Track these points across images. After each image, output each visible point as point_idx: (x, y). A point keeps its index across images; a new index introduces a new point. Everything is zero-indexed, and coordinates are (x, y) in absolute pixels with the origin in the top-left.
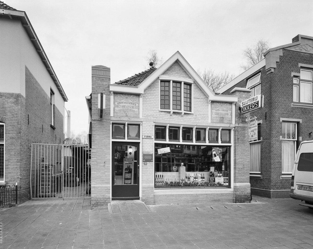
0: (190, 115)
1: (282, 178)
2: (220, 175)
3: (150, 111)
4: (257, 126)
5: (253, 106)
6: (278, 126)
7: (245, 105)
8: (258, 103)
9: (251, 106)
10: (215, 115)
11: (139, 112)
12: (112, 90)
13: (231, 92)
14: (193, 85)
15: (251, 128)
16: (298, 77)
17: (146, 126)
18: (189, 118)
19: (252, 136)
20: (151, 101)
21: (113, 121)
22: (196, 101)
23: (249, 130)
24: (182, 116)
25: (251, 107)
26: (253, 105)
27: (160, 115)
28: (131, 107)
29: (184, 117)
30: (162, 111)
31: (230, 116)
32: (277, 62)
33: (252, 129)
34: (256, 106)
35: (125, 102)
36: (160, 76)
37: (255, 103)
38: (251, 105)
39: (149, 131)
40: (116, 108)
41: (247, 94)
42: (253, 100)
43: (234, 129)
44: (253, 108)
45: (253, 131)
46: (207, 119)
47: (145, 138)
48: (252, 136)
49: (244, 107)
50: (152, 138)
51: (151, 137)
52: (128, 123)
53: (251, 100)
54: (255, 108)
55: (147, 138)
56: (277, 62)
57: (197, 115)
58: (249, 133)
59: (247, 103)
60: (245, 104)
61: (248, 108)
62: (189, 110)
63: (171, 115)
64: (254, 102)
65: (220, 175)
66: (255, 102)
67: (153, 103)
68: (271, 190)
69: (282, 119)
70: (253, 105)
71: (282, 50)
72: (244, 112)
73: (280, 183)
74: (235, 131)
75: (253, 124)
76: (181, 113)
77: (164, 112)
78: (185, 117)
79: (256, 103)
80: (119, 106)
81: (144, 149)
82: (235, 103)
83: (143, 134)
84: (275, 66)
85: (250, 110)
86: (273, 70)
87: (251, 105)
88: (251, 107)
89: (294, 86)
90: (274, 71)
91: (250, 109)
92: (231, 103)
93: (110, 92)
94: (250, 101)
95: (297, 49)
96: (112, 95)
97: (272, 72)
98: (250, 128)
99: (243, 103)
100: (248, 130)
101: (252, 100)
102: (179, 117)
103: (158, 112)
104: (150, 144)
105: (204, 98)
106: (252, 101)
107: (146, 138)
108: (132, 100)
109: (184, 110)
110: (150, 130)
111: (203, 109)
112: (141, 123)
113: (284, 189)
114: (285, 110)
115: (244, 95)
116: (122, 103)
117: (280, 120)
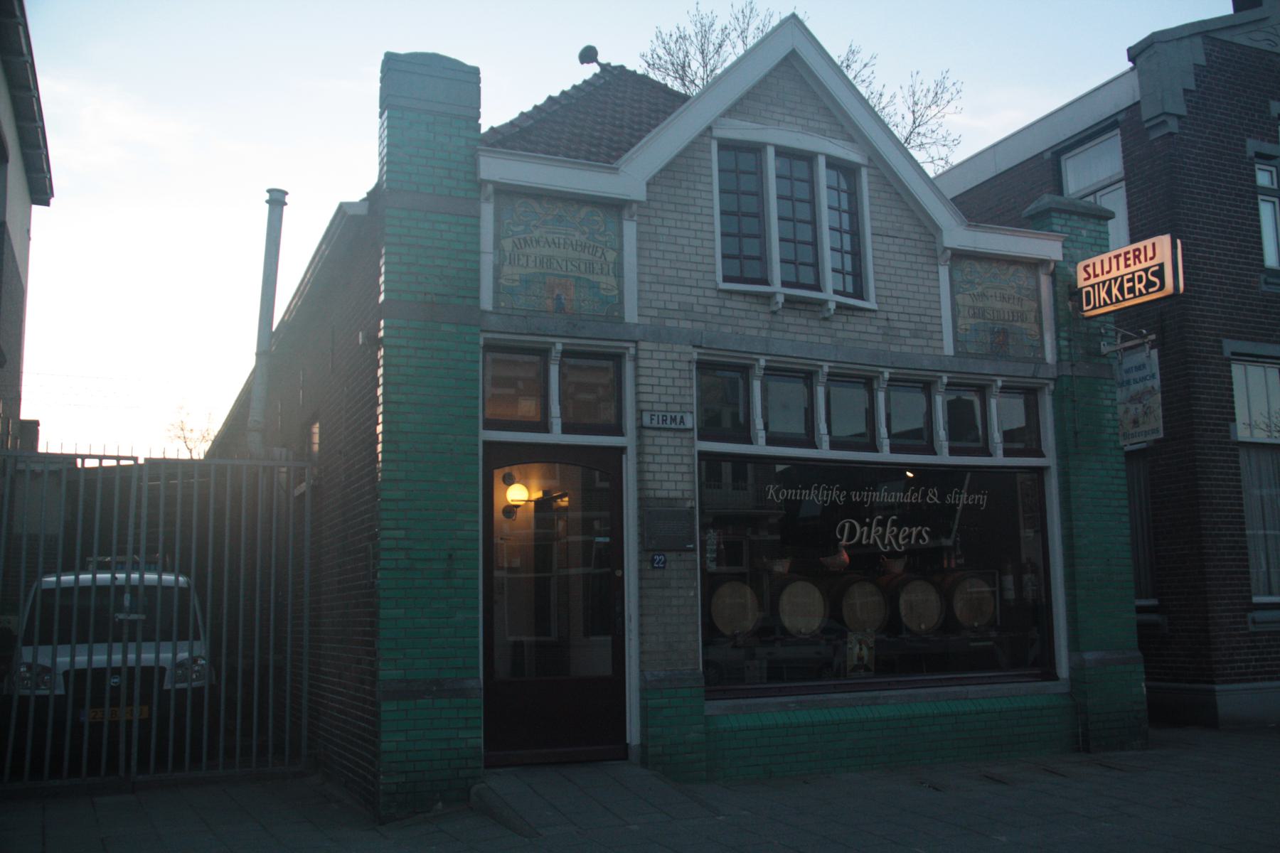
0: (860, 314)
1: (1254, 622)
2: (35, 657)
3: (674, 289)
4: (1158, 376)
5: (1137, 286)
6: (1214, 376)
7: (1101, 279)
8: (1160, 273)
9: (1126, 285)
10: (972, 321)
11: (621, 293)
12: (492, 178)
13: (1026, 212)
14: (864, 172)
15: (1128, 383)
16: (1272, 162)
17: (656, 364)
18: (859, 328)
19: (1135, 423)
20: (680, 241)
21: (489, 335)
22: (884, 247)
23: (1121, 395)
24: (826, 319)
25: (1131, 290)
26: (1140, 282)
27: (724, 312)
28: (583, 267)
29: (835, 326)
30: (730, 292)
31: (1035, 327)
32: (1186, 91)
33: (1135, 388)
34: (1154, 284)
35: (550, 240)
36: (715, 121)
37: (1146, 270)
38: (1128, 281)
39: (670, 391)
40: (507, 270)
41: (1098, 228)
42: (1137, 257)
43: (1052, 387)
44: (1141, 294)
45: (1136, 399)
46: (936, 336)
47: (655, 424)
48: (1135, 423)
49: (1093, 286)
50: (689, 424)
51: (682, 421)
52: (564, 344)
53: (1127, 259)
54: (1148, 293)
55: (673, 426)
56: (1186, 91)
57: (891, 316)
58: (1121, 409)
59: (1106, 268)
60: (1098, 271)
61: (1115, 291)
62: (850, 289)
63: (774, 313)
64: (1139, 266)
65: (35, 657)
66: (1144, 265)
67: (687, 250)
68: (1217, 687)
69: (1229, 346)
70: (1140, 282)
71: (1198, 40)
72: (1094, 308)
73: (1248, 647)
74: (1058, 398)
75: (1141, 367)
76: (823, 303)
77: (741, 298)
78: (840, 326)
79: (1153, 274)
80: (523, 261)
81: (650, 485)
82: (1052, 265)
83: (644, 406)
84: (1183, 111)
85: (1125, 300)
86: (1173, 126)
87: (1128, 281)
88: (1131, 290)
89: (1260, 197)
90: (1180, 128)
91: (1123, 295)
92: (1035, 265)
93: (481, 184)
94: (1122, 260)
95: (1256, 40)
96: (487, 200)
97: (1171, 134)
98: (1121, 385)
99: (1090, 270)
100: (1110, 396)
101: (1131, 255)
102: (812, 323)
103: (714, 294)
104: (678, 460)
105: (916, 236)
106: (1131, 262)
107: (661, 425)
108: (584, 233)
109: (836, 292)
110: (678, 383)
111: (915, 288)
112: (627, 348)
113: (1270, 679)
114: (1237, 303)
115: (1084, 233)
116: (538, 242)
117: (1221, 347)
